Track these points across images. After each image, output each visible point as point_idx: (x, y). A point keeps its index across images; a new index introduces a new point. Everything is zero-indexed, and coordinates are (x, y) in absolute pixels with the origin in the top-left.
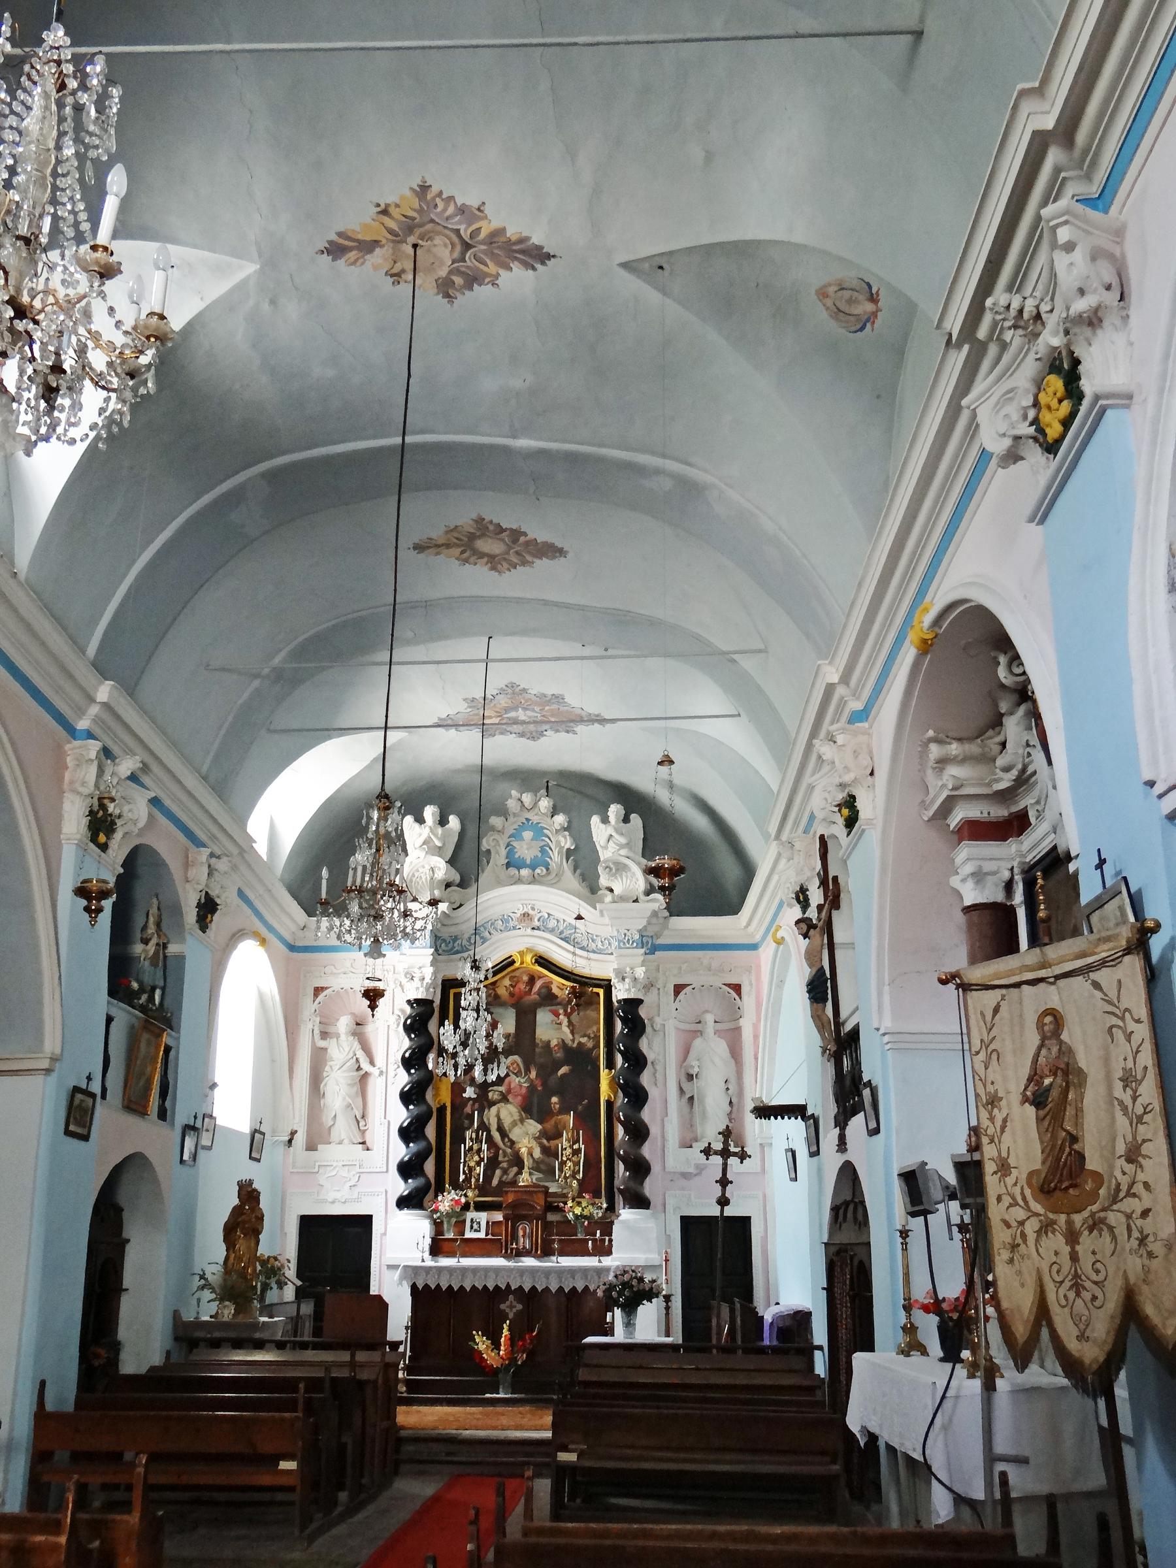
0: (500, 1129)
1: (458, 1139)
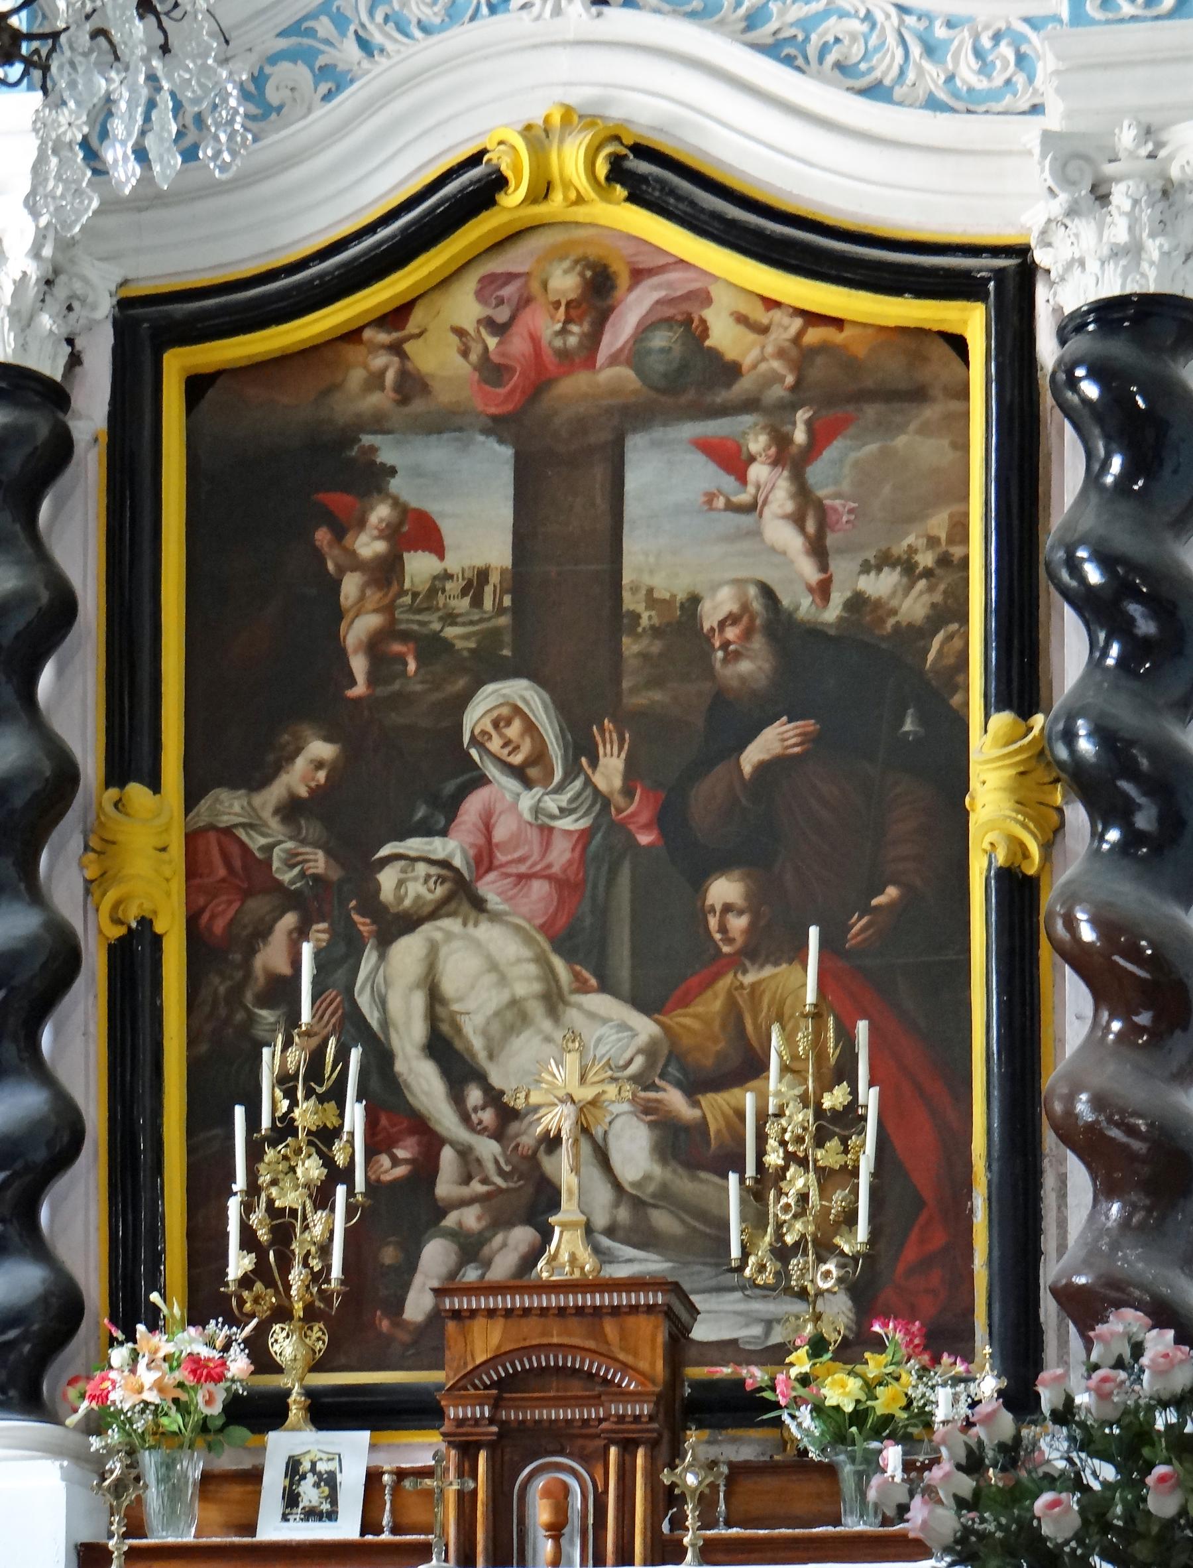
0: (442, 1047)
1: (223, 1078)
